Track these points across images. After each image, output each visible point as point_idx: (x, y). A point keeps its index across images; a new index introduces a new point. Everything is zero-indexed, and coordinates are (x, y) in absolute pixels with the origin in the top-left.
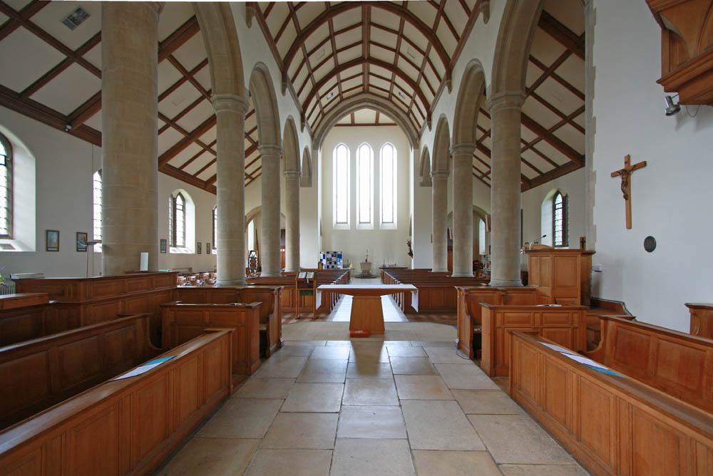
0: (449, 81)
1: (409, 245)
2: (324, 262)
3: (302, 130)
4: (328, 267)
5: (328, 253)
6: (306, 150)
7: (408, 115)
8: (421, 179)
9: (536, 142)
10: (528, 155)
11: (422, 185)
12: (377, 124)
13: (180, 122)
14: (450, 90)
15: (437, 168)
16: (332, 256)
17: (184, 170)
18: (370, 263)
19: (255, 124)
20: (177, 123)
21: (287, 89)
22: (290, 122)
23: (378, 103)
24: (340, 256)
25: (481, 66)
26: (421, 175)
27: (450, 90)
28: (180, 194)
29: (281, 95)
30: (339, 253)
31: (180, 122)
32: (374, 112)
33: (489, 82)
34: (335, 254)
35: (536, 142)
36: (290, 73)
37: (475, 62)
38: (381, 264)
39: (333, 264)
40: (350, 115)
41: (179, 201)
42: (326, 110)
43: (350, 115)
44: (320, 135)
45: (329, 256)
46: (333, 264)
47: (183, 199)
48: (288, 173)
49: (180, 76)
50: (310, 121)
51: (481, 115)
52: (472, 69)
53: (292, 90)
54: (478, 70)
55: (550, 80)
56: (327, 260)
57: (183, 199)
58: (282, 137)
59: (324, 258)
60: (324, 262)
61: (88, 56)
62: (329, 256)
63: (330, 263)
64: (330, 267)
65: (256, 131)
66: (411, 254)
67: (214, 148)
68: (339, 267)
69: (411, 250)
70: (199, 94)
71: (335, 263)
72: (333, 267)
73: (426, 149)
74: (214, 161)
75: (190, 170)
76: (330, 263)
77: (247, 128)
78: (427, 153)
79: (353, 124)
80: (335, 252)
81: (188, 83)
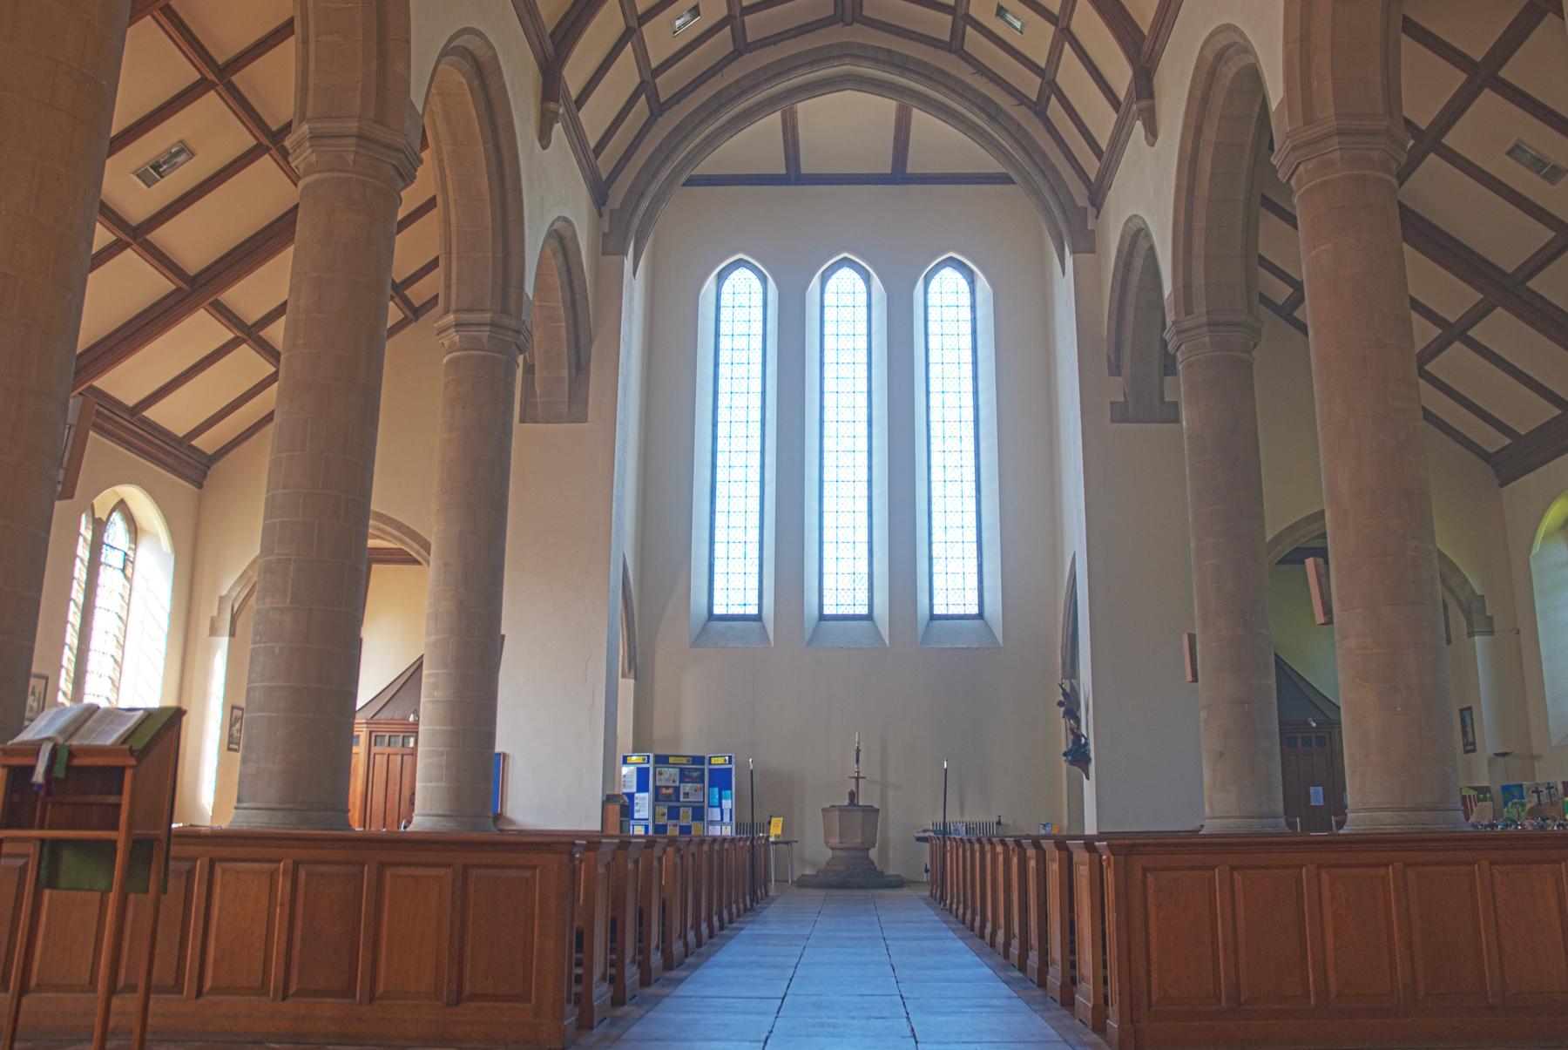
0: (1144, 104)
1: (1071, 708)
2: (643, 805)
3: (544, 137)
4: (661, 829)
5: (661, 760)
6: (561, 239)
7: (1039, 109)
8: (1116, 390)
9: (1476, 315)
10: (1455, 363)
11: (1121, 414)
12: (899, 175)
13: (163, 236)
14: (1152, 132)
15: (1200, 309)
16: (684, 776)
17: (150, 413)
18: (871, 811)
19: (433, 250)
20: (152, 237)
21: (558, 128)
22: (561, 239)
23: (902, 64)
24: (721, 779)
25: (1247, 49)
26: (1115, 369)
27: (1152, 132)
28: (122, 506)
29: (537, 145)
30: (719, 762)
31: (163, 236)
32: (885, 108)
33: (1276, 94)
34: (693, 769)
35: (1476, 315)
36: (574, 75)
37: (1223, 40)
38: (929, 819)
39: (686, 817)
40: (776, 118)
41: (117, 532)
42: (666, 85)
43: (776, 118)
44: (636, 193)
45: (670, 774)
46: (686, 817)
47: (130, 520)
48: (458, 325)
49: (187, 74)
50: (595, 117)
51: (1269, 222)
52: (1220, 56)
53: (576, 133)
54: (1229, 70)
55: (1488, 98)
56: (658, 798)
57: (130, 520)
58: (529, 288)
59: (643, 786)
60: (643, 805)
61: (267, 333)
62: (670, 774)
63: (674, 814)
64: (673, 831)
65: (290, 45)
66: (1078, 755)
67: (276, 333)
68: (715, 831)
69: (1077, 736)
70: (244, 140)
71: (699, 814)
72: (686, 830)
73: (1136, 236)
74: (273, 378)
75: (174, 415)
76: (674, 814)
77: (403, 265)
78: (1142, 245)
79: (793, 176)
80: (699, 760)
81: (211, 101)
